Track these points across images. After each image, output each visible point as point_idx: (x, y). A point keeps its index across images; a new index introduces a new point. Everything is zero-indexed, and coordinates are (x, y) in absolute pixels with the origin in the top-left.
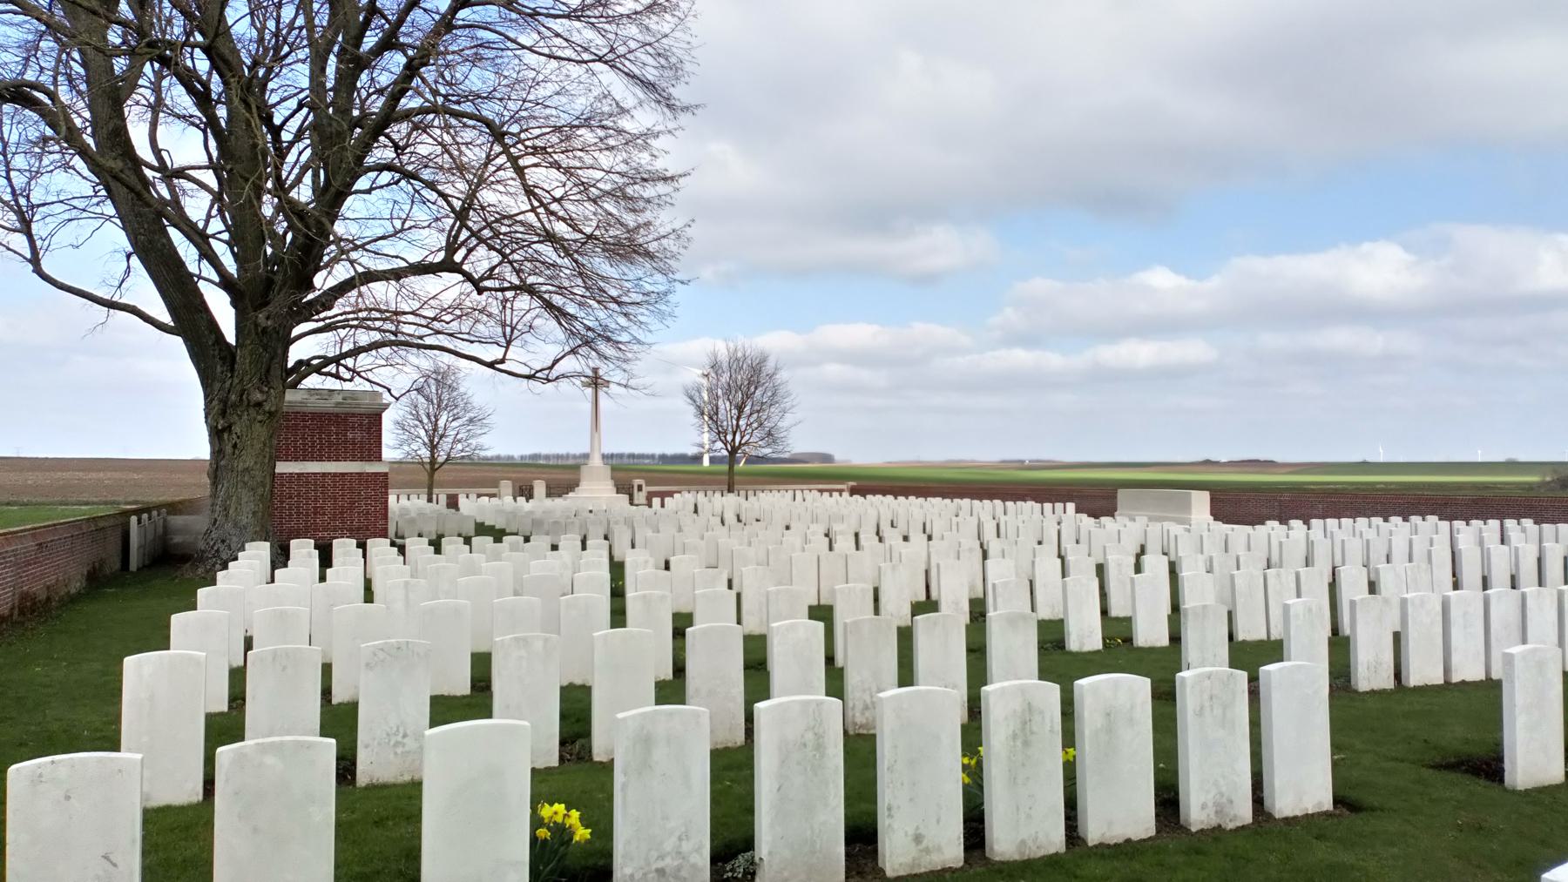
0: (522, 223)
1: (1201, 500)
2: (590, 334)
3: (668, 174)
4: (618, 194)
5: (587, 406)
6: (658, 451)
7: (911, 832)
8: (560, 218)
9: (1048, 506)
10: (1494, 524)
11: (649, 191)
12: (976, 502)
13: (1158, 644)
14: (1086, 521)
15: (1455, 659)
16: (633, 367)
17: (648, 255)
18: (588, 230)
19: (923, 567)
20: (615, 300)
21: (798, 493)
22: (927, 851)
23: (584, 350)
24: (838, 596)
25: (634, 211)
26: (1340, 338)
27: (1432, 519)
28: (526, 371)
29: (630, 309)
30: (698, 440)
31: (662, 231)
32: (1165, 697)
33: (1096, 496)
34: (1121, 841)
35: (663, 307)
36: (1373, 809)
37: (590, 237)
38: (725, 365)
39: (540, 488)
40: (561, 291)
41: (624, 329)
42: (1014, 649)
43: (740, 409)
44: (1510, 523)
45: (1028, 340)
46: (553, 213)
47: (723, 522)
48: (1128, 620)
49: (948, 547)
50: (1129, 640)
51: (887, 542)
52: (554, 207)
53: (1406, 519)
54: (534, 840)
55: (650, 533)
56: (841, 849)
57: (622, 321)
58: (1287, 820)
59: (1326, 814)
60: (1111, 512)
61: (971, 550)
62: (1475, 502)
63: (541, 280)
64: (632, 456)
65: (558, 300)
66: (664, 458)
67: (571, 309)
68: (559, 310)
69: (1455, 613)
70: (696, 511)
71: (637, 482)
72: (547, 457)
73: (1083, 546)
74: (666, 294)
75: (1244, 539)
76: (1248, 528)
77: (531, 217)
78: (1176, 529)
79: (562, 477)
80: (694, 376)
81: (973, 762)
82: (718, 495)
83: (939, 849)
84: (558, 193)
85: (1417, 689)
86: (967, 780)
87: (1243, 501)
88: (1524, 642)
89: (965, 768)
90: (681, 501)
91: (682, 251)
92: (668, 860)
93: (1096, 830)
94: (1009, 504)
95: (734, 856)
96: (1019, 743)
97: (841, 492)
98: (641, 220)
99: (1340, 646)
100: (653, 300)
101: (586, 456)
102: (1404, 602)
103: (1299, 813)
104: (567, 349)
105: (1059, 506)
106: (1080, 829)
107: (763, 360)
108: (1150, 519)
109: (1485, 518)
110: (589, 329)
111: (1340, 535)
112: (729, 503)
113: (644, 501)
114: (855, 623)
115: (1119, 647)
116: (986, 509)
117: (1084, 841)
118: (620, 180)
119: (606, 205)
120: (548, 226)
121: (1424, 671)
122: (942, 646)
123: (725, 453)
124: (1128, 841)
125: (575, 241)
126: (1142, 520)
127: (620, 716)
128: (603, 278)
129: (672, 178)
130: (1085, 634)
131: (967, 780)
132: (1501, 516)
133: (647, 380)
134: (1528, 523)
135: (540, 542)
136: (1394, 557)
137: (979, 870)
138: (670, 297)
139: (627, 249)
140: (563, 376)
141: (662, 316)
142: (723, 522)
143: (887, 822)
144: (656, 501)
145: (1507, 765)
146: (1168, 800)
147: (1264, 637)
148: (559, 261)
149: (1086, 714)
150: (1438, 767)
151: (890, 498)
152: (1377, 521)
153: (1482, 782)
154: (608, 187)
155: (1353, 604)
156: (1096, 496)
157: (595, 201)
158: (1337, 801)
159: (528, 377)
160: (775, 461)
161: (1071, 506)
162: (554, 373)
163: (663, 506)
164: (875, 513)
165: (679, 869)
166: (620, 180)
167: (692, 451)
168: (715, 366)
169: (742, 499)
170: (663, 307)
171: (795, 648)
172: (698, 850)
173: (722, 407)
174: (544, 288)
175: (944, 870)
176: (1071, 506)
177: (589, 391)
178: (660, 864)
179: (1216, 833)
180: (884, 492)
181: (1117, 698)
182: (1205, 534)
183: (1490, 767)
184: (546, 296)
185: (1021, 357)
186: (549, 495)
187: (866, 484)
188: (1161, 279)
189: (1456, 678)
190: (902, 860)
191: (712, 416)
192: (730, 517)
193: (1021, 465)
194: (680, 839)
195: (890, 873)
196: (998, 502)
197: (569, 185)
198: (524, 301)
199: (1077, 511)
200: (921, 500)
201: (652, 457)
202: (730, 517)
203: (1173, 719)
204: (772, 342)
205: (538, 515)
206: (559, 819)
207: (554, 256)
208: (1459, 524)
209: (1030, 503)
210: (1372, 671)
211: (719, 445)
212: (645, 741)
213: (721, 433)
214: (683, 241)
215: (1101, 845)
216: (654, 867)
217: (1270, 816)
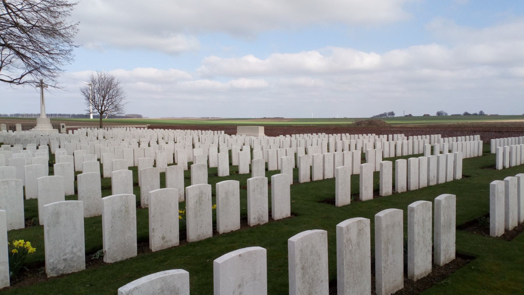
0: (4, 19)
1: (262, 129)
2: (37, 65)
3: (68, 3)
4: (47, 10)
5: (39, 95)
6: (71, 113)
7: (161, 236)
8: (20, 17)
9: (216, 132)
10: (339, 135)
11: (60, 9)
12: (192, 131)
13: (246, 173)
14: (227, 136)
15: (326, 172)
16: (57, 79)
17: (60, 34)
18: (34, 23)
19: (172, 152)
20: (47, 52)
21: (128, 129)
22: (167, 241)
23: (35, 72)
24: (140, 162)
25: (54, 17)
26: (302, 80)
27: (324, 134)
28: (9, 80)
29: (54, 56)
30: (87, 109)
31: (67, 26)
32: (243, 188)
33: (230, 129)
34: (229, 231)
35: (69, 56)
36: (301, 215)
37: (34, 26)
38: (97, 81)
39: (19, 127)
40: (23, 47)
41: (51, 64)
42: (200, 176)
43: (104, 97)
44: (343, 135)
45: (210, 77)
46: (17, 15)
47: (97, 139)
48: (237, 166)
49: (183, 146)
50: (237, 172)
51: (160, 144)
52: (18, 13)
53: (317, 134)
54: (10, 254)
55: (66, 143)
56: (136, 245)
57: (50, 60)
58: (278, 220)
59: (289, 218)
60: (235, 133)
61: (189, 146)
62: (335, 129)
63: (14, 43)
64: (60, 115)
65: (22, 51)
66: (74, 116)
67: (28, 55)
68: (22, 55)
69: (326, 159)
70: (87, 135)
71: (62, 124)
72: (22, 115)
73: (226, 144)
74: (70, 51)
75: (273, 141)
76: (274, 138)
77: (8, 16)
78: (253, 138)
79: (29, 123)
80: (85, 84)
81: (183, 212)
82: (96, 129)
83: (171, 241)
84: (19, 7)
85: (316, 181)
86: (181, 218)
87: (273, 130)
88: (343, 165)
89: (180, 214)
90: (81, 132)
91: (75, 34)
92: (68, 256)
93: (222, 228)
94: (203, 131)
95: (96, 252)
96: (198, 204)
97: (144, 128)
98: (57, 21)
99: (296, 170)
100: (62, 53)
101: (39, 115)
102: (313, 156)
103: (281, 218)
104: (27, 71)
105: (219, 132)
106: (217, 229)
107: (113, 79)
108: (247, 135)
109: (337, 133)
110: (36, 63)
111: (299, 139)
112: (101, 132)
113: (66, 132)
114: (145, 170)
115: (234, 172)
116: (195, 133)
117: (218, 233)
118: (48, 4)
119: (42, 14)
120: (15, 20)
121: (318, 176)
122: (176, 178)
123: (98, 114)
124: (232, 231)
125: (28, 27)
126: (244, 136)
127: (45, 206)
128: (41, 43)
129: (70, 5)
130: (224, 170)
131: (181, 218)
132: (341, 133)
133: (64, 85)
134: (348, 134)
135: (17, 147)
136: (313, 144)
137: (184, 245)
138: (71, 52)
139: (52, 32)
140: (26, 82)
141: (68, 60)
142: (97, 139)
143: (152, 234)
144: (70, 132)
145: (336, 200)
146: (244, 217)
147: (276, 169)
148: (21, 35)
149: (219, 193)
150: (319, 202)
151: (162, 130)
152: (310, 135)
153: (330, 205)
154: (42, 6)
155: (300, 157)
156: (230, 129)
157: (37, 12)
158: (292, 213)
159: (11, 82)
160: (119, 117)
161: (223, 132)
162: (22, 80)
163: (73, 133)
164: (156, 135)
165: (73, 258)
166: (48, 4)
167: (85, 113)
168: (93, 81)
169: (106, 131)
170: (69, 56)
171: (122, 180)
172: (80, 251)
173: (96, 96)
174: (16, 46)
175: (172, 247)
176: (223, 132)
177: (39, 89)
178: (65, 257)
179: (258, 226)
180: (160, 128)
181: (229, 188)
182: (262, 139)
183: (332, 201)
184: (17, 49)
185: (207, 83)
186: (23, 129)
187: (153, 125)
188: (252, 61)
189: (326, 178)
190: (158, 245)
191: (91, 99)
192: (101, 137)
193: (208, 119)
194: (72, 248)
195: (153, 250)
196: (199, 131)
197: (24, 4)
198: (7, 51)
199: (225, 133)
200: (173, 130)
201: (69, 115)
202: (101, 137)
203: (246, 194)
204: (117, 73)
205: (18, 137)
206: (22, 245)
207: (19, 33)
208: (330, 135)
209: (210, 131)
210: (304, 178)
211: (96, 110)
212: (57, 214)
213: (96, 106)
214: (75, 30)
215: (224, 233)
216: (62, 258)
217: (273, 220)
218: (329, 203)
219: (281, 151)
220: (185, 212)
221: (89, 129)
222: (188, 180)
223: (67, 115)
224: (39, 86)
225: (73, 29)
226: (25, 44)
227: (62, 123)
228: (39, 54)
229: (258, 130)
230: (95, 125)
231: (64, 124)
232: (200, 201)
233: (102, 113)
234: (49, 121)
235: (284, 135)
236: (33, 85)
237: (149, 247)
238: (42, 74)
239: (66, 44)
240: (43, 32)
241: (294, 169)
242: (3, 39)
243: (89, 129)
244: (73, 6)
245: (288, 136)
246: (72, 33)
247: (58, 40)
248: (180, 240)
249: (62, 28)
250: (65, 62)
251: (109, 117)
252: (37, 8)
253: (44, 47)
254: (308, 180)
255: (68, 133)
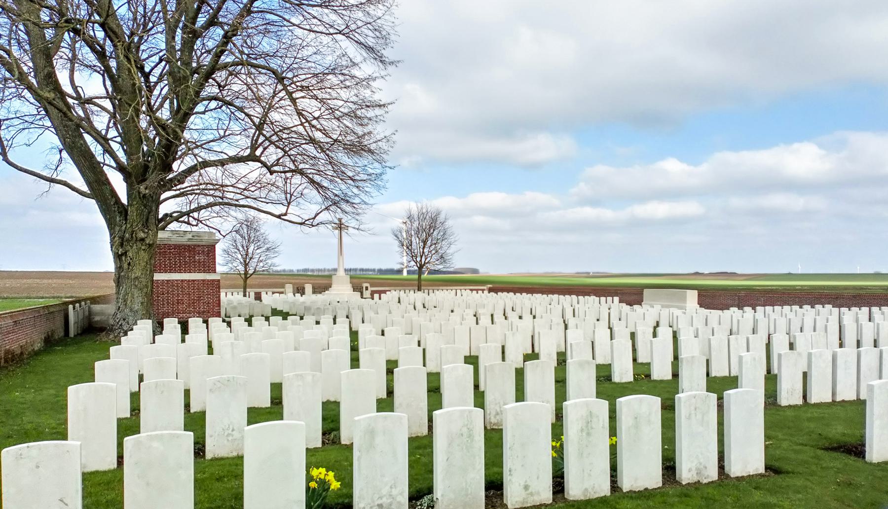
0: (296, 132)
1: (692, 296)
2: (336, 198)
3: (382, 103)
4: (352, 115)
5: (336, 241)
6: (377, 267)
7: (522, 484)
9: (603, 299)
10: (865, 309)
11: (371, 113)
12: (561, 297)
13: (666, 378)
14: (625, 307)
17: (370, 151)
18: (335, 137)
19: (531, 334)
20: (351, 178)
22: (532, 494)
23: (333, 208)
24: (481, 350)
25: (362, 125)
26: (776, 200)
27: (828, 307)
28: (300, 220)
29: (360, 184)
32: (668, 407)
35: (379, 183)
36: (788, 473)
37: (335, 141)
38: (416, 217)
39: (308, 288)
42: (582, 380)
43: (425, 242)
44: (875, 309)
45: (594, 202)
46: (313, 126)
50: (648, 376)
51: (510, 319)
52: (314, 122)
53: (813, 307)
54: (308, 488)
55: (372, 314)
56: (483, 493)
57: (355, 190)
58: (738, 479)
60: (639, 302)
61: (558, 324)
63: (307, 166)
65: (317, 178)
66: (381, 271)
67: (325, 183)
68: (318, 184)
71: (365, 285)
73: (623, 322)
74: (381, 175)
75: (716, 319)
78: (677, 312)
80: (398, 223)
81: (558, 445)
82: (412, 292)
83: (538, 493)
84: (317, 114)
89: (553, 448)
90: (391, 296)
91: (390, 149)
94: (581, 298)
95: (422, 497)
96: (584, 434)
97: (483, 290)
99: (771, 379)
101: (335, 270)
104: (323, 207)
105: (609, 299)
108: (663, 306)
109: (860, 306)
110: (336, 195)
111: (773, 316)
112: (418, 297)
116: (567, 300)
117: (621, 490)
118: (353, 107)
119: (345, 122)
120: (310, 134)
123: (416, 268)
124: (646, 489)
126: (658, 307)
127: (356, 418)
129: (384, 105)
130: (623, 373)
131: (555, 455)
132: (870, 305)
133: (371, 226)
135: (309, 319)
136: (805, 329)
138: (383, 176)
139: (357, 148)
140: (321, 223)
141: (378, 188)
143: (509, 478)
144: (376, 296)
145: (867, 449)
146: (669, 468)
148: (318, 155)
149: (623, 417)
150: (826, 449)
152: (796, 308)
153: (852, 458)
154: (346, 111)
155: (780, 356)
156: (632, 295)
157: (338, 119)
158: (767, 468)
159: (301, 224)
160: (445, 273)
161: (616, 299)
162: (316, 222)
167: (397, 267)
168: (410, 217)
170: (379, 183)
171: (457, 381)
172: (401, 494)
174: (309, 171)
175: (541, 505)
176: (616, 299)
177: (337, 232)
178: (380, 502)
179: (697, 485)
180: (508, 290)
181: (641, 409)
182: (694, 315)
184: (311, 176)
185: (588, 212)
186: (314, 292)
187: (498, 287)
189: (838, 399)
192: (419, 306)
193: (588, 275)
194: (391, 488)
196: (574, 297)
197: (323, 109)
198: (297, 179)
200: (530, 295)
201: (374, 270)
202: (419, 306)
203: (673, 420)
204: (444, 204)
205: (308, 304)
206: (322, 477)
207: (315, 152)
208: (844, 310)
209: (593, 297)
210: (789, 394)
211: (413, 263)
213: (413, 257)
217: (728, 476)
218: (850, 454)
219: (735, 340)
220: (562, 446)
221: (402, 292)
222: (561, 384)
223: (371, 270)
224: (336, 229)
225: (388, 141)
226: (322, 169)
227: (370, 283)
228: (340, 181)
229: (685, 297)
230: (412, 285)
231: (368, 285)
232: (587, 429)
233: (421, 267)
234: (349, 279)
235: (740, 307)
236: (330, 227)
237: (502, 499)
238: (343, 211)
239: (376, 165)
240: (346, 149)
241: (766, 378)
242: (294, 162)
243: (402, 292)
244: (389, 107)
245: (748, 309)
246: (386, 148)
247: (365, 160)
248: (554, 493)
249: (372, 141)
250: (374, 192)
251: (429, 273)
252: (339, 114)
253: (346, 171)
254: (798, 401)
255: (373, 299)
